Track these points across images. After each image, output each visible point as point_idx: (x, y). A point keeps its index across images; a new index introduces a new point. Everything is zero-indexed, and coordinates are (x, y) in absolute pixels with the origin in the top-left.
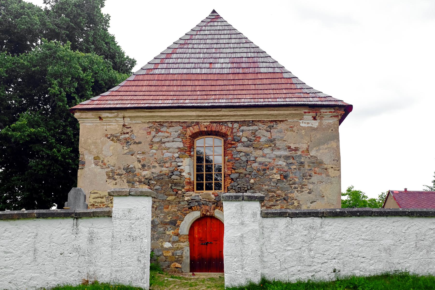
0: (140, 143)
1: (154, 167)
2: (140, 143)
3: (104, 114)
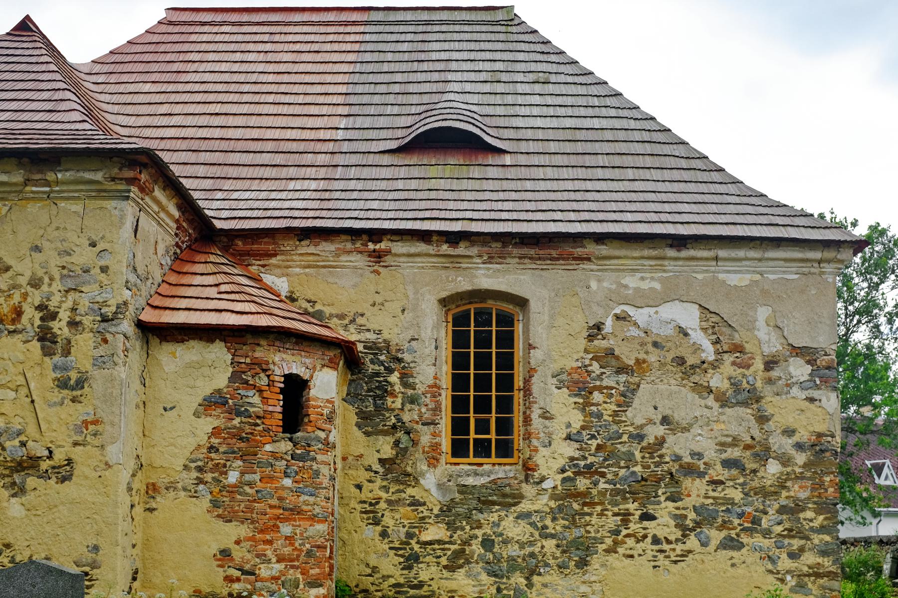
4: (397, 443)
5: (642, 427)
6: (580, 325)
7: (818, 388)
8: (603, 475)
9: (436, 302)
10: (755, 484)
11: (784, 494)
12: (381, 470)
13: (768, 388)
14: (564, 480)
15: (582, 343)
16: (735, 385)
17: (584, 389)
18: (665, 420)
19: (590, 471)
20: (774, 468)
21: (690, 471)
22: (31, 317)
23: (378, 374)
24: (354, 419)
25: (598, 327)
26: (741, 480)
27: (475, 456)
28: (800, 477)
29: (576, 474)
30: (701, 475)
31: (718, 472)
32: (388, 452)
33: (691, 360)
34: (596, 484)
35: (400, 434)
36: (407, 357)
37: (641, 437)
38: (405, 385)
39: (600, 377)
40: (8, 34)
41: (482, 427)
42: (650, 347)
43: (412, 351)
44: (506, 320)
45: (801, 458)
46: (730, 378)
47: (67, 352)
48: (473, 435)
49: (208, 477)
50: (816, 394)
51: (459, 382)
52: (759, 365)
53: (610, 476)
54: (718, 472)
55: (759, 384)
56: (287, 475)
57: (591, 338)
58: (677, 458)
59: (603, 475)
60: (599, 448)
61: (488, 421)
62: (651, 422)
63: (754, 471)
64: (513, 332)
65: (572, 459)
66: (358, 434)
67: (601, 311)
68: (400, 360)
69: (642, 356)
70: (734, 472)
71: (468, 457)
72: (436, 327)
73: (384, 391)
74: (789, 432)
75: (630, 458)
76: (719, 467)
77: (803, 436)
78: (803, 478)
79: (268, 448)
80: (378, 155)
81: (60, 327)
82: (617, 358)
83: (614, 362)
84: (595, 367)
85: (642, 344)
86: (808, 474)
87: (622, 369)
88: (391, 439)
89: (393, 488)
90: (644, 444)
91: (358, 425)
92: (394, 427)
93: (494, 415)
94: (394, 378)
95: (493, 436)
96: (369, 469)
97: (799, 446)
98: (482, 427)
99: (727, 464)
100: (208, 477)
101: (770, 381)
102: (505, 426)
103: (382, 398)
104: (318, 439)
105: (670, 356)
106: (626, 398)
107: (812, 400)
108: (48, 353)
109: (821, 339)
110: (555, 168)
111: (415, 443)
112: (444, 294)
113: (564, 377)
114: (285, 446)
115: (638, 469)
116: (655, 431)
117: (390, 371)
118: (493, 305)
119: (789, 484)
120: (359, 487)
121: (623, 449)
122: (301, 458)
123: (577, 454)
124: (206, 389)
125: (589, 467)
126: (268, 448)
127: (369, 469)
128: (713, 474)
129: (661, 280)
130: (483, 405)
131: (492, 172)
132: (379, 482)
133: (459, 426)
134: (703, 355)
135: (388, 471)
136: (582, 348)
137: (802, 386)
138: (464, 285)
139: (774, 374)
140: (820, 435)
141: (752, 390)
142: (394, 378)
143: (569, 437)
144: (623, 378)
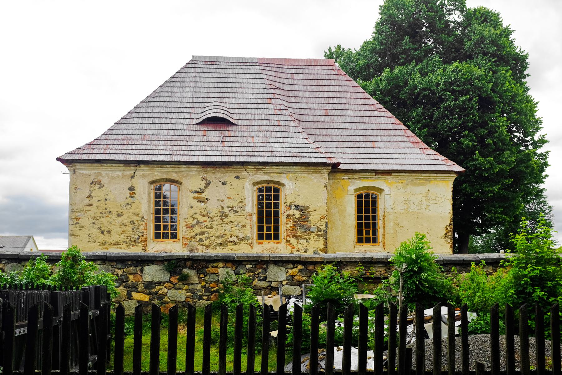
9: (147, 183)
27: (163, 238)
40: (172, 77)
41: (269, 229)
44: (277, 190)
48: (265, 232)
51: (260, 213)
61: (369, 231)
64: (279, 195)
71: (264, 240)
80: (195, 125)
93: (371, 229)
95: (371, 236)
98: (269, 229)
102: (374, 233)
110: (321, 130)
118: (273, 185)
130: (269, 222)
131: (232, 134)
133: (260, 229)
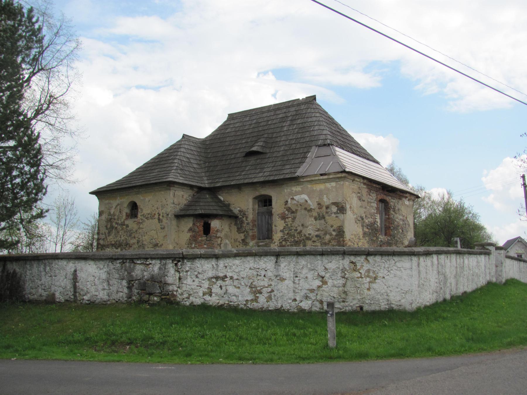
0: (364, 201)
1: (369, 218)
2: (364, 201)
3: (357, 179)
4: (245, 235)
5: (296, 227)
6: (283, 202)
7: (338, 213)
8: (288, 241)
10: (323, 241)
11: (330, 244)
12: (241, 242)
13: (327, 215)
14: (280, 243)
15: (284, 206)
16: (319, 215)
17: (283, 218)
18: (303, 225)
19: (285, 240)
20: (328, 237)
21: (308, 239)
22: (157, 216)
23: (241, 218)
24: (236, 230)
25: (287, 202)
26: (320, 241)
28: (335, 239)
29: (283, 241)
30: (310, 239)
31: (315, 239)
32: (243, 238)
33: (308, 209)
34: (287, 243)
35: (245, 233)
36: (246, 213)
37: (296, 230)
38: (247, 220)
39: (287, 215)
42: (299, 206)
43: (247, 212)
45: (334, 233)
46: (317, 213)
47: (162, 222)
49: (189, 246)
50: (338, 215)
52: (324, 208)
53: (290, 241)
54: (315, 239)
55: (324, 214)
56: (205, 245)
57: (286, 204)
58: (305, 235)
59: (288, 241)
60: (288, 233)
62: (299, 226)
63: (323, 238)
65: (282, 237)
66: (237, 233)
67: (287, 197)
68: (245, 214)
69: (297, 208)
70: (318, 238)
72: (253, 205)
73: (242, 222)
74: (332, 226)
75: (294, 236)
76: (315, 237)
77: (335, 227)
78: (336, 239)
79: (200, 239)
81: (161, 217)
82: (291, 209)
83: (290, 211)
84: (287, 212)
85: (297, 205)
86: (336, 238)
87: (293, 212)
88: (244, 234)
89: (244, 247)
90: (298, 232)
91: (237, 231)
92: (244, 231)
94: (244, 219)
96: (239, 242)
97: (334, 230)
99: (317, 236)
100: (189, 246)
101: (327, 213)
103: (242, 224)
104: (214, 236)
105: (303, 208)
106: (294, 219)
107: (337, 217)
108: (159, 222)
109: (340, 199)
111: (248, 234)
112: (254, 197)
113: (280, 215)
114: (204, 238)
115: (296, 239)
116: (299, 229)
117: (243, 217)
119: (331, 241)
120: (237, 246)
121: (292, 233)
122: (209, 241)
123: (282, 236)
124: (189, 228)
125: (285, 239)
126: (200, 239)
127: (239, 242)
128: (313, 239)
129: (301, 188)
132: (241, 245)
134: (311, 207)
135: (243, 242)
136: (283, 207)
137: (335, 213)
138: (257, 194)
139: (329, 210)
140: (339, 227)
141: (323, 215)
142: (244, 219)
143: (281, 231)
144: (293, 215)
